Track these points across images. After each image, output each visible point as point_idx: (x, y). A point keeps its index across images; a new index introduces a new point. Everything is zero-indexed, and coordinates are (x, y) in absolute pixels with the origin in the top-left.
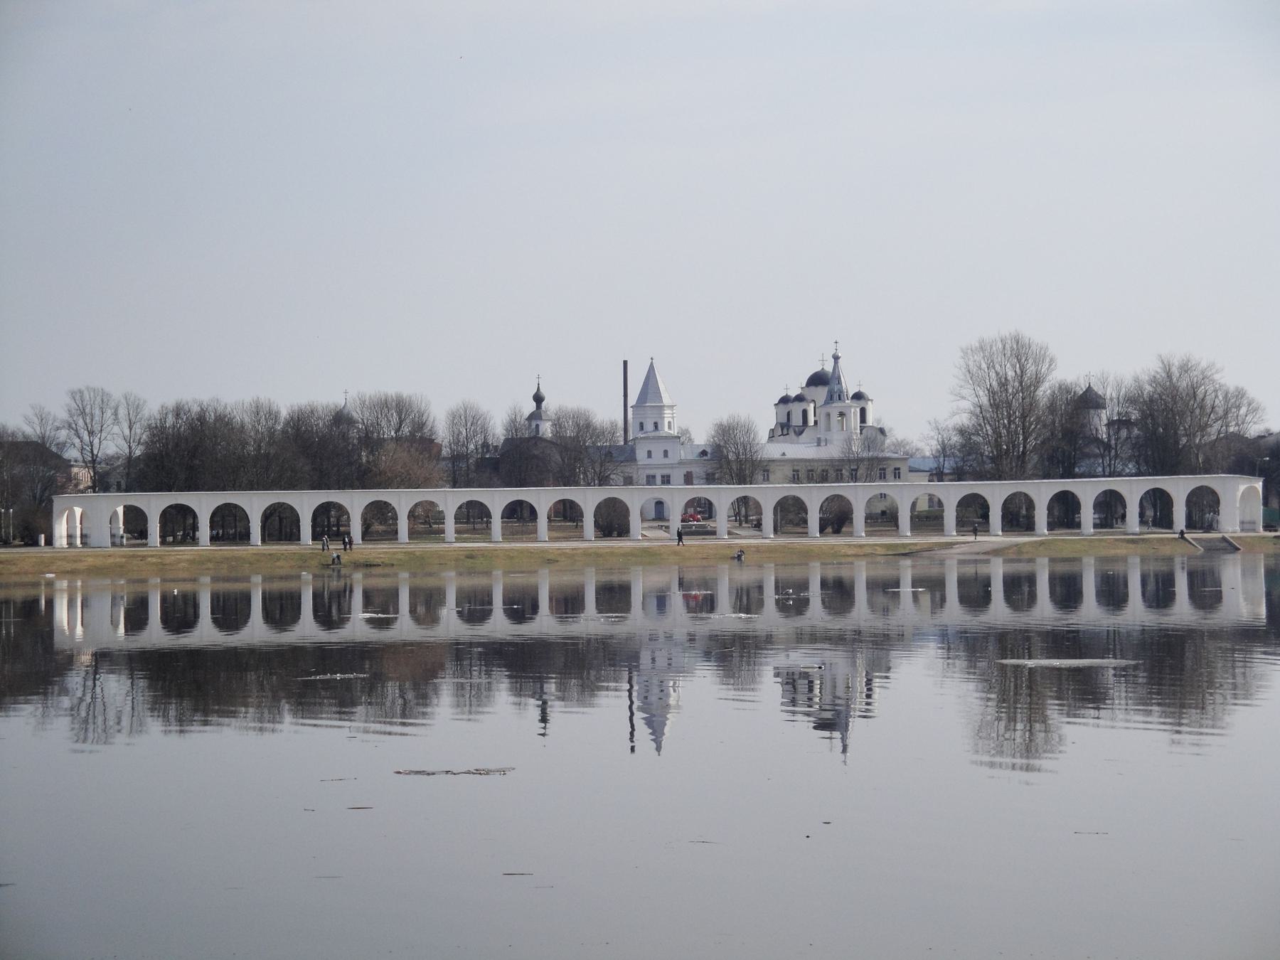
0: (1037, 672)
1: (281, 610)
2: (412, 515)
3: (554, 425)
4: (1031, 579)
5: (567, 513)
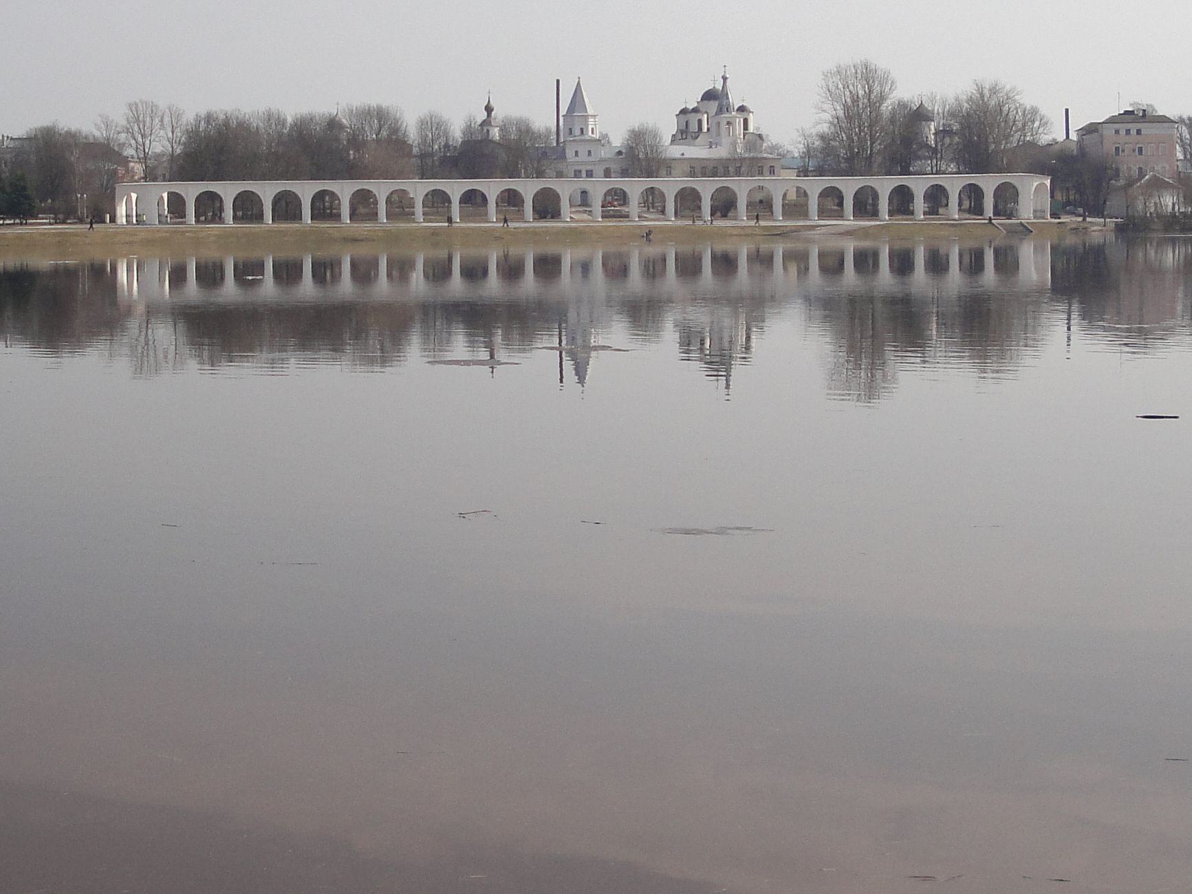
0: (878, 326)
1: (288, 273)
2: (388, 201)
3: (501, 130)
4: (876, 255)
5: (511, 199)
